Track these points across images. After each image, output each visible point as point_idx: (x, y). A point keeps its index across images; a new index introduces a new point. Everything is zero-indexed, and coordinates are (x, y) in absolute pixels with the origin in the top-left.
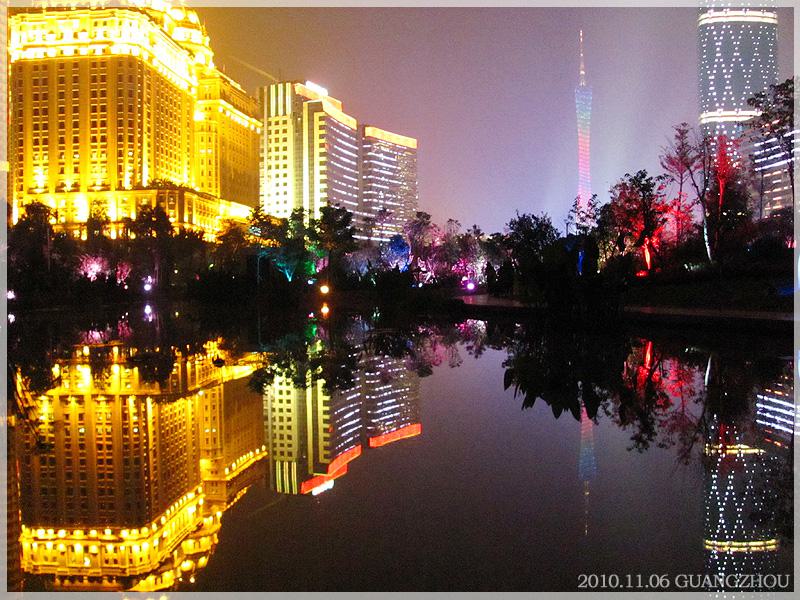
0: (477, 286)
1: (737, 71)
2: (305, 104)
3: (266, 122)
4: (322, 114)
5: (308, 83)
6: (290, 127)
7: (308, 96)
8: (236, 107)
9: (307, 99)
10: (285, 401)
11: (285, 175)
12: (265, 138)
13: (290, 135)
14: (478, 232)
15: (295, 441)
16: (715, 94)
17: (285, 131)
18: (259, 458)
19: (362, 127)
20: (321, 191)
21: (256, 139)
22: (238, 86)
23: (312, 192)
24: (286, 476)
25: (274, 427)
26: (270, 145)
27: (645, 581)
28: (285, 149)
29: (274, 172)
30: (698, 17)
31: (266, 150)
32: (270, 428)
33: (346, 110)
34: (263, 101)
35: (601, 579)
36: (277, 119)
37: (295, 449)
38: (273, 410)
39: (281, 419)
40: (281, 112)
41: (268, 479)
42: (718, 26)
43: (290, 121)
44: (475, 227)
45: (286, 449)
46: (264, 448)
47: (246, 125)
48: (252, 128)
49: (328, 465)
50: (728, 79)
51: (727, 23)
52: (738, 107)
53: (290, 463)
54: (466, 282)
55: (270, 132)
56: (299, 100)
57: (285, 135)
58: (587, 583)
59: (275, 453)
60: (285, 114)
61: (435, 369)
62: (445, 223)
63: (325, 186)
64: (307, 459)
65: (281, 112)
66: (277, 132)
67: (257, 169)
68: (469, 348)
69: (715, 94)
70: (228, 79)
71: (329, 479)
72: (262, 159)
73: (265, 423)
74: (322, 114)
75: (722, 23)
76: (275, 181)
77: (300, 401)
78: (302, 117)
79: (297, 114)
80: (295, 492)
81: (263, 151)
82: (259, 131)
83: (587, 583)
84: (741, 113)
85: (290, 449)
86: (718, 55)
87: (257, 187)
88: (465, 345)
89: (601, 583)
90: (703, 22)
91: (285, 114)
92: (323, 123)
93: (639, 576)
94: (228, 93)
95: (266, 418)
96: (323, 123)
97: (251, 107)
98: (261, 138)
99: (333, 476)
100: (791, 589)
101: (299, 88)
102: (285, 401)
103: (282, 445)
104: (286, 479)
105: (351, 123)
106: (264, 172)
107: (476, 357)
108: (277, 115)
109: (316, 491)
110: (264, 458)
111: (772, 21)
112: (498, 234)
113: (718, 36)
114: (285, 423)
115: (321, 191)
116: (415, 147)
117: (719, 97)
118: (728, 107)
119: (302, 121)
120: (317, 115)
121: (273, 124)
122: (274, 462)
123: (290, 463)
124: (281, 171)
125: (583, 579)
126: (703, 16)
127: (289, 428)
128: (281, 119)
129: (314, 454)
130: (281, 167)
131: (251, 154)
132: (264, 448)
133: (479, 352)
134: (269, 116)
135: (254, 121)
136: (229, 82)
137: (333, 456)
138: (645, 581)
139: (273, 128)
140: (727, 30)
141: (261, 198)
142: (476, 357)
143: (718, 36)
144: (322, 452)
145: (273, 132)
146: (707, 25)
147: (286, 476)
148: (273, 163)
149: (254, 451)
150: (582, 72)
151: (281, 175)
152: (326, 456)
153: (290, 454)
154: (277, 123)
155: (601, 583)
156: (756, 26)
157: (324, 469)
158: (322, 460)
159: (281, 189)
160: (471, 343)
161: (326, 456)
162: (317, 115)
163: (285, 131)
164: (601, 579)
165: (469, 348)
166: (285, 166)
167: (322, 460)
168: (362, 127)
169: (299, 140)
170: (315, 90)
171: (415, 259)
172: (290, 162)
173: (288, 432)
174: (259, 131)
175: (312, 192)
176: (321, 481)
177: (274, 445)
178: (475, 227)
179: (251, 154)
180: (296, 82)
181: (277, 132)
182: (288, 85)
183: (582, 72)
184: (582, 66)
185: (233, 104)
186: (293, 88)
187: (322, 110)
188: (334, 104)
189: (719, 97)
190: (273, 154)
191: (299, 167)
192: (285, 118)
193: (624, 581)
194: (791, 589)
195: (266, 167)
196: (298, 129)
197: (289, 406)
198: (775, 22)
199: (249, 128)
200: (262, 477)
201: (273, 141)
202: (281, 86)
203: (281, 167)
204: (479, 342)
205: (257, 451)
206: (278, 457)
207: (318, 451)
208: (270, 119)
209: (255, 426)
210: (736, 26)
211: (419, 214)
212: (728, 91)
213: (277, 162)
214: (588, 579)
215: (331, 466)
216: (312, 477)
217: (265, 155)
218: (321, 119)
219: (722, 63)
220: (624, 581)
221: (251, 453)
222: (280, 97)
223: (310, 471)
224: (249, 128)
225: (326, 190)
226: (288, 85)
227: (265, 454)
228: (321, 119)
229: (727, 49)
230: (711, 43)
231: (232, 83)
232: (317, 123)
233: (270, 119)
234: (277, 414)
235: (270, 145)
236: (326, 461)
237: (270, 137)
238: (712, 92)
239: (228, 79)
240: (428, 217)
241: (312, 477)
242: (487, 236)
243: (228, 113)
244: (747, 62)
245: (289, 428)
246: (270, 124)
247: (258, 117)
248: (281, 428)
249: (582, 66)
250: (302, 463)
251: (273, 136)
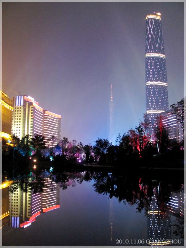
0: (82, 161)
1: (157, 99)
2: (27, 103)
3: (15, 108)
4: (32, 106)
5: (28, 96)
6: (22, 110)
7: (28, 100)
8: (6, 102)
9: (28, 101)
10: (16, 197)
11: (19, 130)
12: (14, 112)
13: (22, 112)
14: (81, 144)
15: (19, 210)
16: (151, 105)
17: (20, 119)
18: (7, 216)
19: (44, 111)
20: (31, 130)
21: (11, 113)
22: (7, 96)
23: (28, 130)
24: (15, 222)
25: (12, 205)
26: (16, 115)
27: (137, 242)
28: (20, 125)
29: (16, 123)
30: (146, 83)
31: (14, 114)
32: (11, 206)
33: (39, 105)
34: (14, 101)
35: (125, 242)
36: (18, 107)
37: (19, 213)
38: (12, 200)
39: (14, 209)
40: (19, 105)
41: (9, 223)
42: (151, 85)
43: (22, 108)
44: (81, 143)
45: (16, 213)
46: (8, 212)
47: (8, 108)
48: (10, 109)
49: (29, 218)
50: (157, 91)
51: (154, 85)
52: (157, 109)
53: (17, 217)
54: (78, 160)
55: (16, 111)
56: (25, 101)
57: (20, 115)
58: (119, 242)
59: (12, 214)
60: (21, 105)
61: (68, 186)
62: (72, 141)
63: (32, 128)
64: (22, 216)
65: (19, 105)
66: (17, 122)
67: (11, 122)
68: (78, 181)
69: (151, 105)
70: (4, 94)
71: (30, 222)
72: (13, 119)
73: (9, 204)
74: (32, 106)
75: (153, 85)
76: (16, 126)
77: (21, 197)
78: (26, 107)
79: (24, 106)
80: (18, 227)
81: (13, 117)
82: (12, 110)
83: (119, 242)
84: (158, 111)
85: (17, 207)
86: (152, 94)
87: (11, 128)
88: (77, 180)
89: (123, 242)
90: (147, 84)
91: (21, 105)
92: (32, 109)
93: (135, 240)
94: (3, 98)
95: (10, 202)
96: (32, 109)
97: (11, 103)
98: (13, 113)
99: (31, 222)
100: (182, 244)
101: (26, 97)
102: (16, 197)
103: (14, 211)
104: (15, 222)
105: (41, 109)
106: (13, 123)
107: (80, 184)
108: (18, 106)
109: (25, 226)
110: (8, 216)
111: (166, 85)
112: (88, 145)
113: (152, 88)
114: (16, 210)
115: (31, 130)
116: (61, 118)
117: (152, 106)
118: (155, 109)
119: (26, 108)
120: (31, 107)
121: (17, 108)
122: (12, 217)
123: (17, 217)
124: (18, 123)
125: (117, 241)
126: (147, 83)
127: (17, 209)
128: (19, 107)
129: (25, 203)
130: (18, 127)
131: (9, 117)
132: (8, 212)
133: (81, 182)
134: (16, 106)
135: (11, 107)
136: (4, 94)
137: (31, 216)
138: (137, 242)
139: (17, 110)
140: (154, 87)
141: (12, 131)
142: (80, 184)
143: (152, 88)
144: (28, 214)
145: (17, 111)
146: (148, 85)
147: (15, 222)
148: (16, 120)
149: (5, 213)
150: (112, 97)
151: (18, 130)
152: (29, 215)
153: (17, 214)
154: (18, 108)
155: (123, 242)
156: (162, 86)
157: (28, 219)
158: (27, 216)
159: (18, 129)
160: (79, 179)
161: (29, 215)
162: (31, 107)
163: (20, 125)
164: (125, 242)
165: (78, 181)
166: (19, 130)
167: (27, 216)
168: (44, 111)
169: (24, 114)
170: (30, 99)
171: (63, 152)
172: (21, 120)
173: (17, 210)
174: (12, 110)
175: (28, 130)
176: (27, 223)
177: (12, 211)
178: (81, 143)
179: (9, 117)
180: (25, 96)
181: (18, 111)
182: (22, 97)
183: (112, 97)
184: (112, 95)
185: (5, 101)
186: (24, 98)
187: (32, 105)
188: (36, 103)
189: (152, 106)
190: (16, 118)
191: (24, 122)
192: (21, 107)
193: (130, 242)
194: (182, 244)
195: (14, 122)
196: (25, 110)
197: (17, 198)
198: (167, 86)
199: (9, 109)
200: (7, 222)
201: (17, 114)
202: (20, 97)
203: (18, 127)
204: (82, 179)
205: (6, 213)
206: (13, 216)
207: (27, 199)
208: (16, 107)
209: (6, 204)
210: (156, 86)
211: (64, 138)
212: (154, 104)
213: (17, 120)
214: (119, 241)
215: (30, 218)
216: (24, 222)
217: (14, 118)
218: (32, 108)
219: (153, 96)
220: (130, 242)
221: (4, 214)
222: (19, 101)
223: (24, 220)
224: (9, 109)
225: (32, 130)
226: (22, 97)
227: (9, 214)
228: (32, 108)
229: (154, 93)
230: (149, 90)
231: (5, 95)
232: (31, 109)
233: (16, 107)
234: (13, 201)
235: (16, 115)
236: (29, 217)
237: (16, 112)
238: (150, 104)
239: (4, 94)
240: (67, 139)
241: (24, 222)
242: (84, 146)
243: (3, 104)
244: (160, 96)
245: (17, 203)
246: (16, 108)
247: (12, 106)
248: (14, 209)
249: (112, 95)
250: (21, 217)
251: (17, 112)
